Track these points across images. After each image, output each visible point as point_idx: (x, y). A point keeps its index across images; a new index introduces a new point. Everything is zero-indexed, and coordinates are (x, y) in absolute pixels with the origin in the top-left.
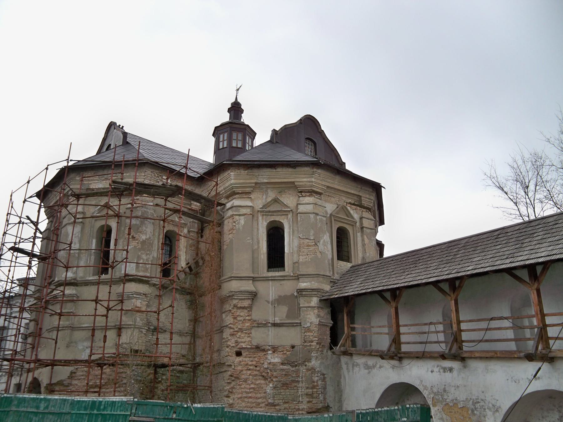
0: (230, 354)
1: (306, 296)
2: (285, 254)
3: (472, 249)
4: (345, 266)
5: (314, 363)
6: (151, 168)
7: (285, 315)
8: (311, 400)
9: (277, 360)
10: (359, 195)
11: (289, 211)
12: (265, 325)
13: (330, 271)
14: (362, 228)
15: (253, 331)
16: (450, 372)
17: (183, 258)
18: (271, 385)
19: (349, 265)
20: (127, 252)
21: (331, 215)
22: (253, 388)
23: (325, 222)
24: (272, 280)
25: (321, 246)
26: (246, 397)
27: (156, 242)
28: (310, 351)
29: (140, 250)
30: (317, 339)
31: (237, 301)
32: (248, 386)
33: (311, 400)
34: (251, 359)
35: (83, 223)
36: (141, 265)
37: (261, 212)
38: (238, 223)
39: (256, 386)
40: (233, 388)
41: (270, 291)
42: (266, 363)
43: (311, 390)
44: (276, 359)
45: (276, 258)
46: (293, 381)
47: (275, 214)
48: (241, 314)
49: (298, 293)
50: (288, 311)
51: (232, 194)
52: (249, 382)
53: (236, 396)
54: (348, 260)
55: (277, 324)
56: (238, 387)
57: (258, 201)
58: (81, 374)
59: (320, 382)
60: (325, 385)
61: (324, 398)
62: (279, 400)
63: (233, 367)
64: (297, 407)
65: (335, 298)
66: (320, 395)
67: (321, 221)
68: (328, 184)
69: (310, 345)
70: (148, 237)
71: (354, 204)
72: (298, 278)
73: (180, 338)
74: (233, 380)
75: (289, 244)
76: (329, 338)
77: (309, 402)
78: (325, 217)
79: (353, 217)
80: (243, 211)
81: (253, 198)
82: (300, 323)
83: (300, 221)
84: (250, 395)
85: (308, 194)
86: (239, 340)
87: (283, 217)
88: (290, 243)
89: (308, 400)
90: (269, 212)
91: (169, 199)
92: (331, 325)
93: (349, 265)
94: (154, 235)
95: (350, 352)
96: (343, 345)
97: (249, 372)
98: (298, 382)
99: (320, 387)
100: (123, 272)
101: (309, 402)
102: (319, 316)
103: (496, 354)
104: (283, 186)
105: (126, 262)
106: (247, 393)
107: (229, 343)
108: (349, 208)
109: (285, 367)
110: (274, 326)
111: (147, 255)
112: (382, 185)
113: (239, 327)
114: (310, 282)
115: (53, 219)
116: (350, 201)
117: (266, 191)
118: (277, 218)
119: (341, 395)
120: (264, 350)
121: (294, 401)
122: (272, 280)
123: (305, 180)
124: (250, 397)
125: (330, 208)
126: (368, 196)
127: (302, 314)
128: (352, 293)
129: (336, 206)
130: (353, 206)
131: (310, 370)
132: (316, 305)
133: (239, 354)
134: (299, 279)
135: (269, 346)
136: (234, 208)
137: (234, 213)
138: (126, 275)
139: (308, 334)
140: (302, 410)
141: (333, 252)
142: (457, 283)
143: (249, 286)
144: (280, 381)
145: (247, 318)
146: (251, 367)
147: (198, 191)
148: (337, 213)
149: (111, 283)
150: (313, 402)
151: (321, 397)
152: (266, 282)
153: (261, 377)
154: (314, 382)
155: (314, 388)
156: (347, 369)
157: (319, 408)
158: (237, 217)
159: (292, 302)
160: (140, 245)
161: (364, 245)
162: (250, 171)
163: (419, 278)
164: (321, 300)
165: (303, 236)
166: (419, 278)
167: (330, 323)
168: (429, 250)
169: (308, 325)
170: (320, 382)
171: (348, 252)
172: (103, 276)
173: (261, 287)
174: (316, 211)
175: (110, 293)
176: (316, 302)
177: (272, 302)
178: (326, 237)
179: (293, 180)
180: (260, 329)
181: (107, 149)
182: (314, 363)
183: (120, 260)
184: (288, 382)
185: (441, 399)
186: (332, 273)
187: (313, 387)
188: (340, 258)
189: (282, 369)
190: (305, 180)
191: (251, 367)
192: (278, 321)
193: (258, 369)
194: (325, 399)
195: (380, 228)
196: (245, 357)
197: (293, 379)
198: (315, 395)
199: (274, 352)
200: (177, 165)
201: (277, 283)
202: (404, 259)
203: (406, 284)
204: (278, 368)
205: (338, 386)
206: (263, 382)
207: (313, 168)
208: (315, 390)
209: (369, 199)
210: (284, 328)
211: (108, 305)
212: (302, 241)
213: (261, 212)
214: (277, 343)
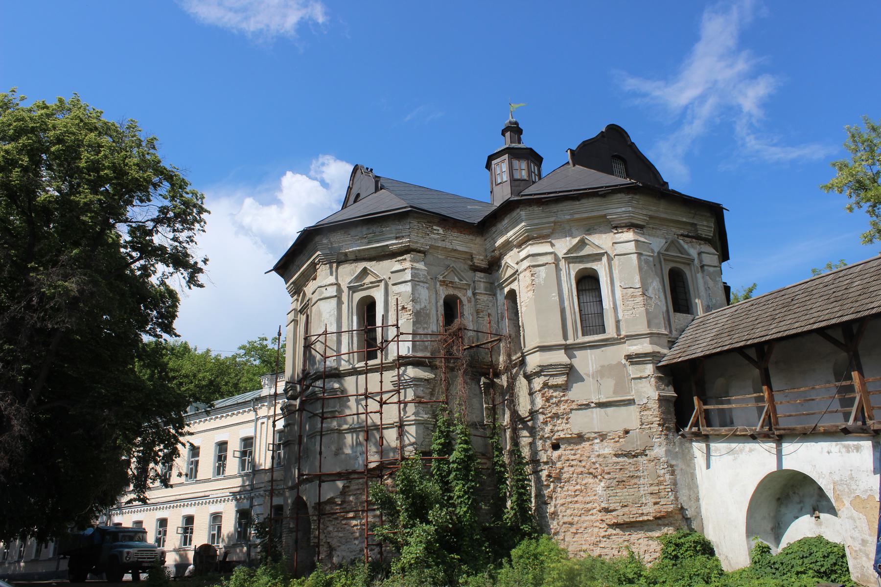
3: (873, 278)
6: (417, 218)
7: (612, 390)
8: (658, 500)
9: (607, 451)
11: (603, 254)
12: (587, 406)
14: (702, 267)
16: (857, 451)
20: (398, 328)
21: (659, 253)
23: (652, 264)
27: (433, 312)
34: (573, 452)
38: (538, 277)
43: (657, 488)
44: (607, 449)
48: (554, 394)
50: (616, 385)
58: (356, 487)
59: (668, 476)
64: (640, 512)
68: (650, 213)
69: (650, 428)
70: (423, 306)
71: (687, 236)
77: (656, 503)
79: (688, 254)
89: (654, 500)
94: (430, 303)
96: (696, 424)
99: (668, 483)
100: (396, 354)
101: (656, 503)
105: (398, 341)
108: (681, 242)
109: (621, 459)
112: (724, 206)
113: (554, 411)
115: (299, 296)
116: (682, 232)
120: (588, 439)
123: (619, 210)
126: (705, 223)
128: (702, 354)
129: (664, 241)
135: (595, 433)
138: (400, 357)
139: (645, 413)
141: (667, 303)
142: (766, 348)
148: (666, 250)
149: (382, 369)
157: (670, 510)
163: (797, 325)
166: (797, 325)
168: (805, 286)
169: (645, 401)
171: (686, 300)
172: (370, 363)
175: (381, 382)
176: (652, 370)
177: (593, 375)
179: (601, 213)
180: (580, 412)
181: (355, 201)
183: (390, 339)
184: (625, 479)
185: (847, 490)
187: (659, 484)
188: (677, 309)
190: (619, 210)
192: (603, 400)
194: (676, 499)
195: (724, 265)
197: (631, 474)
198: (662, 494)
199: (602, 441)
201: (597, 351)
202: (770, 302)
203: (780, 335)
204: (610, 461)
211: (381, 399)
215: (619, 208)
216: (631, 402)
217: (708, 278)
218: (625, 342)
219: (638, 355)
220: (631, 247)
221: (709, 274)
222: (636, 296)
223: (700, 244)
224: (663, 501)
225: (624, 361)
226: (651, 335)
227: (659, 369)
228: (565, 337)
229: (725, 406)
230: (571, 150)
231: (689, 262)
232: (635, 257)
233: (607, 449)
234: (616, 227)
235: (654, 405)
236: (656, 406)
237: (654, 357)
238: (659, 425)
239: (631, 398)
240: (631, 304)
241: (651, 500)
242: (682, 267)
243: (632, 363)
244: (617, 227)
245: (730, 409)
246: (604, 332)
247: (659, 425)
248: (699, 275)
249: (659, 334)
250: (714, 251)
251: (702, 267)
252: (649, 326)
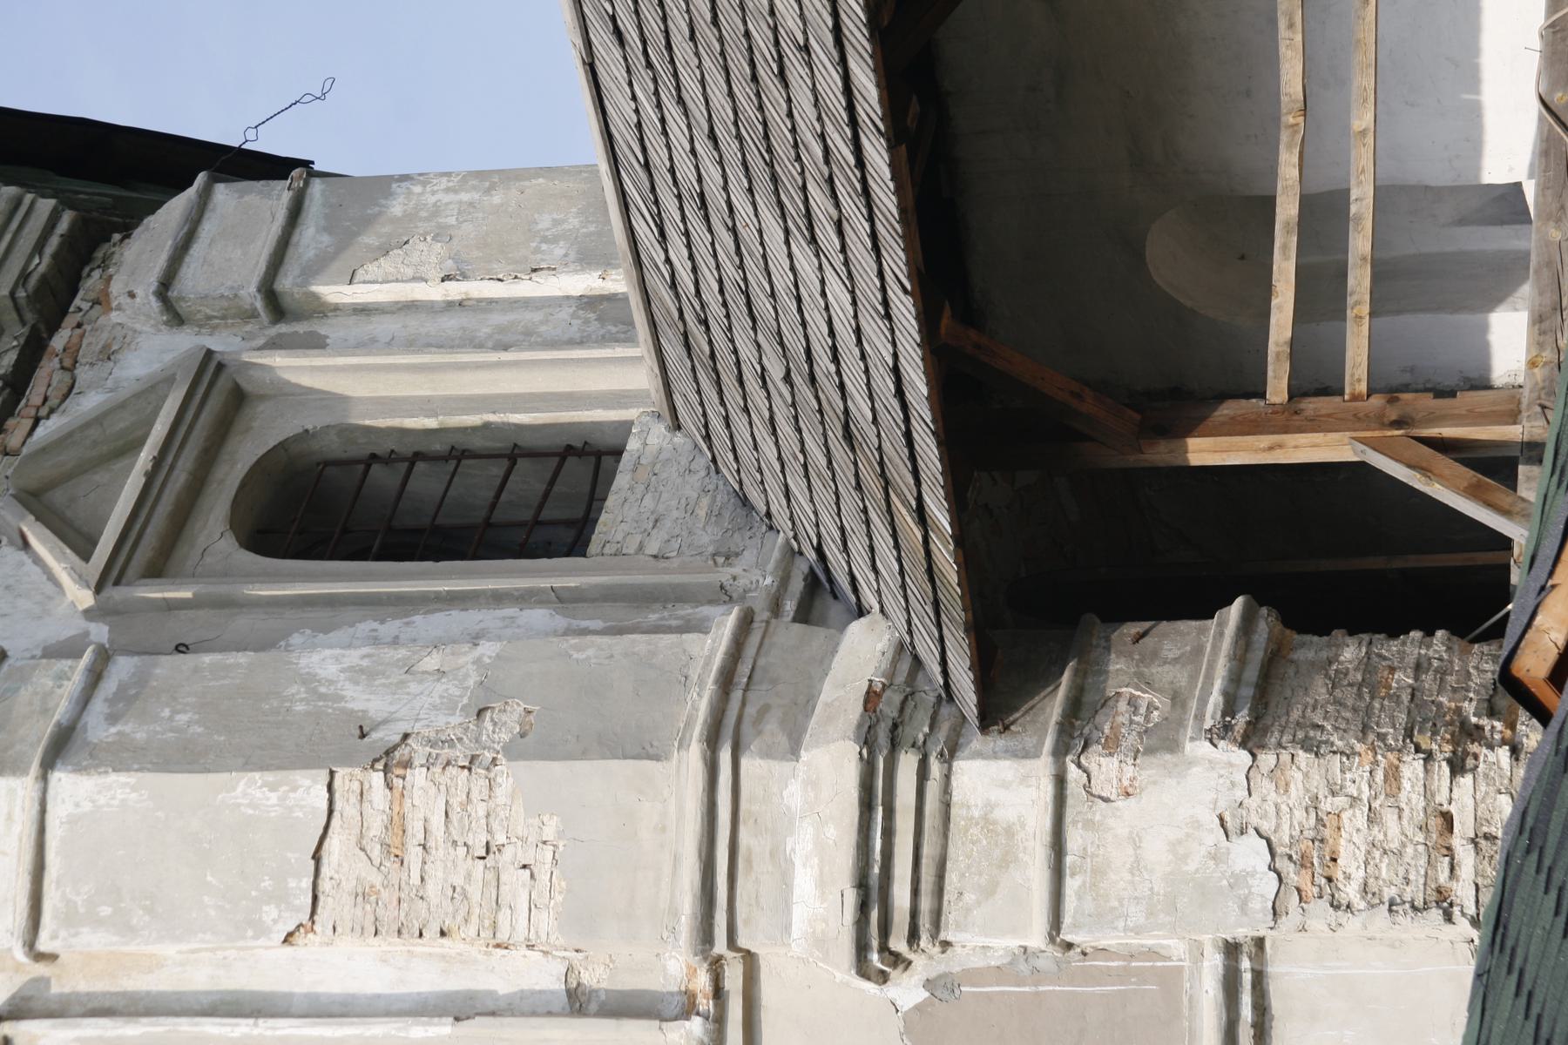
13: (700, 627)
65: (961, 539)
78: (104, 657)
79: (153, 390)
102: (1161, 741)
128: (905, 309)
130: (34, 395)
132: (1043, 767)
139: (1350, 863)
141: (498, 599)
165: (280, 897)
169: (1250, 854)
176: (1006, 768)
188: (569, 535)
216: (1245, 974)
218: (750, 959)
219: (870, 891)
222: (397, 824)
223: (101, 301)
225: (907, 990)
226: (724, 733)
227: (996, 711)
232: (72, 789)
235: (1293, 786)
236: (1304, 773)
237: (891, 726)
238: (1457, 767)
239: (1214, 963)
240: (447, 869)
242: (244, 453)
243: (928, 924)
245: (1384, 196)
246: (1518, 185)
247: (1457, 767)
249: (726, 680)
250: (177, 207)
252: (646, 748)
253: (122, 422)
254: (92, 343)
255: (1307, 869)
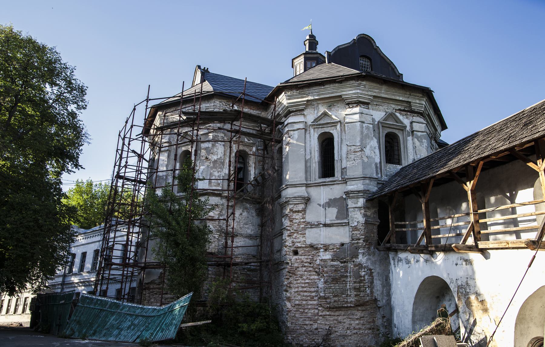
0: (288, 253)
1: (353, 198)
2: (335, 162)
4: (394, 168)
5: (362, 259)
6: (219, 99)
7: (335, 216)
8: (359, 293)
10: (407, 102)
15: (307, 232)
17: (253, 172)
18: (322, 280)
19: (399, 167)
21: (378, 122)
22: (307, 283)
23: (371, 129)
24: (323, 185)
25: (367, 151)
26: (302, 291)
28: (357, 248)
29: (212, 168)
30: (363, 237)
31: (292, 206)
32: (303, 281)
33: (359, 293)
34: (306, 257)
35: (170, 151)
36: (213, 181)
37: (312, 125)
39: (310, 281)
40: (290, 283)
41: (322, 194)
42: (318, 260)
43: (358, 285)
44: (327, 256)
45: (327, 167)
46: (342, 276)
47: (325, 126)
48: (297, 217)
49: (346, 195)
51: (288, 113)
52: (305, 278)
53: (293, 290)
54: (399, 162)
55: (328, 224)
56: (295, 282)
57: (310, 116)
60: (373, 279)
61: (371, 291)
62: (329, 293)
63: (290, 264)
66: (367, 289)
67: (368, 128)
68: (374, 94)
69: (358, 243)
70: (219, 157)
71: (404, 110)
72: (345, 181)
73: (250, 241)
74: (290, 276)
75: (338, 152)
76: (376, 235)
77: (356, 295)
79: (402, 123)
80: (296, 126)
81: (306, 114)
82: (348, 223)
83: (348, 130)
84: (305, 289)
85: (355, 105)
86: (295, 240)
87: (333, 128)
88: (340, 151)
89: (355, 293)
90: (320, 125)
91: (234, 123)
92: (378, 223)
93: (399, 167)
94: (224, 155)
95: (393, 248)
97: (304, 269)
98: (347, 277)
103: (508, 244)
104: (332, 100)
106: (303, 287)
107: (287, 244)
110: (325, 226)
111: (218, 172)
114: (357, 184)
117: (318, 106)
118: (327, 130)
119: (390, 289)
120: (317, 249)
121: (343, 294)
122: (323, 185)
124: (306, 292)
125: (378, 115)
126: (418, 101)
127: (350, 215)
129: (385, 113)
131: (357, 266)
133: (296, 253)
134: (346, 183)
135: (322, 244)
136: (289, 125)
137: (290, 129)
139: (356, 232)
140: (351, 302)
141: (380, 156)
143: (301, 191)
144: (330, 276)
145: (302, 220)
146: (306, 264)
147: (263, 114)
150: (361, 295)
151: (368, 291)
152: (319, 187)
153: (314, 273)
154: (361, 277)
155: (361, 283)
156: (394, 264)
158: (292, 132)
159: (341, 204)
160: (212, 164)
161: (415, 147)
162: (301, 90)
164: (367, 201)
165: (350, 143)
167: (377, 222)
169: (356, 224)
170: (366, 277)
173: (314, 192)
174: (363, 120)
178: (374, 143)
180: (313, 229)
182: (362, 259)
184: (337, 277)
185: (464, 292)
186: (380, 175)
187: (360, 282)
189: (332, 266)
191: (306, 264)
192: (328, 222)
193: (312, 265)
194: (372, 292)
196: (301, 255)
200: (236, 91)
205: (386, 280)
206: (316, 277)
207: (358, 81)
208: (362, 284)
209: (419, 104)
210: (334, 228)
212: (349, 148)
213: (312, 125)
214: (328, 242)
215: (350, 91)
217: (416, 140)
220: (357, 117)
221: (418, 138)
222: (356, 152)
224: (362, 294)
226: (364, 178)
228: (306, 180)
229: (404, 229)
230: (328, 52)
231: (403, 128)
233: (327, 256)
234: (348, 104)
241: (354, 293)
242: (396, 132)
244: (349, 104)
248: (410, 138)
251: (413, 132)
253: (398, 120)
254: (409, 116)
255: (355, 228)
